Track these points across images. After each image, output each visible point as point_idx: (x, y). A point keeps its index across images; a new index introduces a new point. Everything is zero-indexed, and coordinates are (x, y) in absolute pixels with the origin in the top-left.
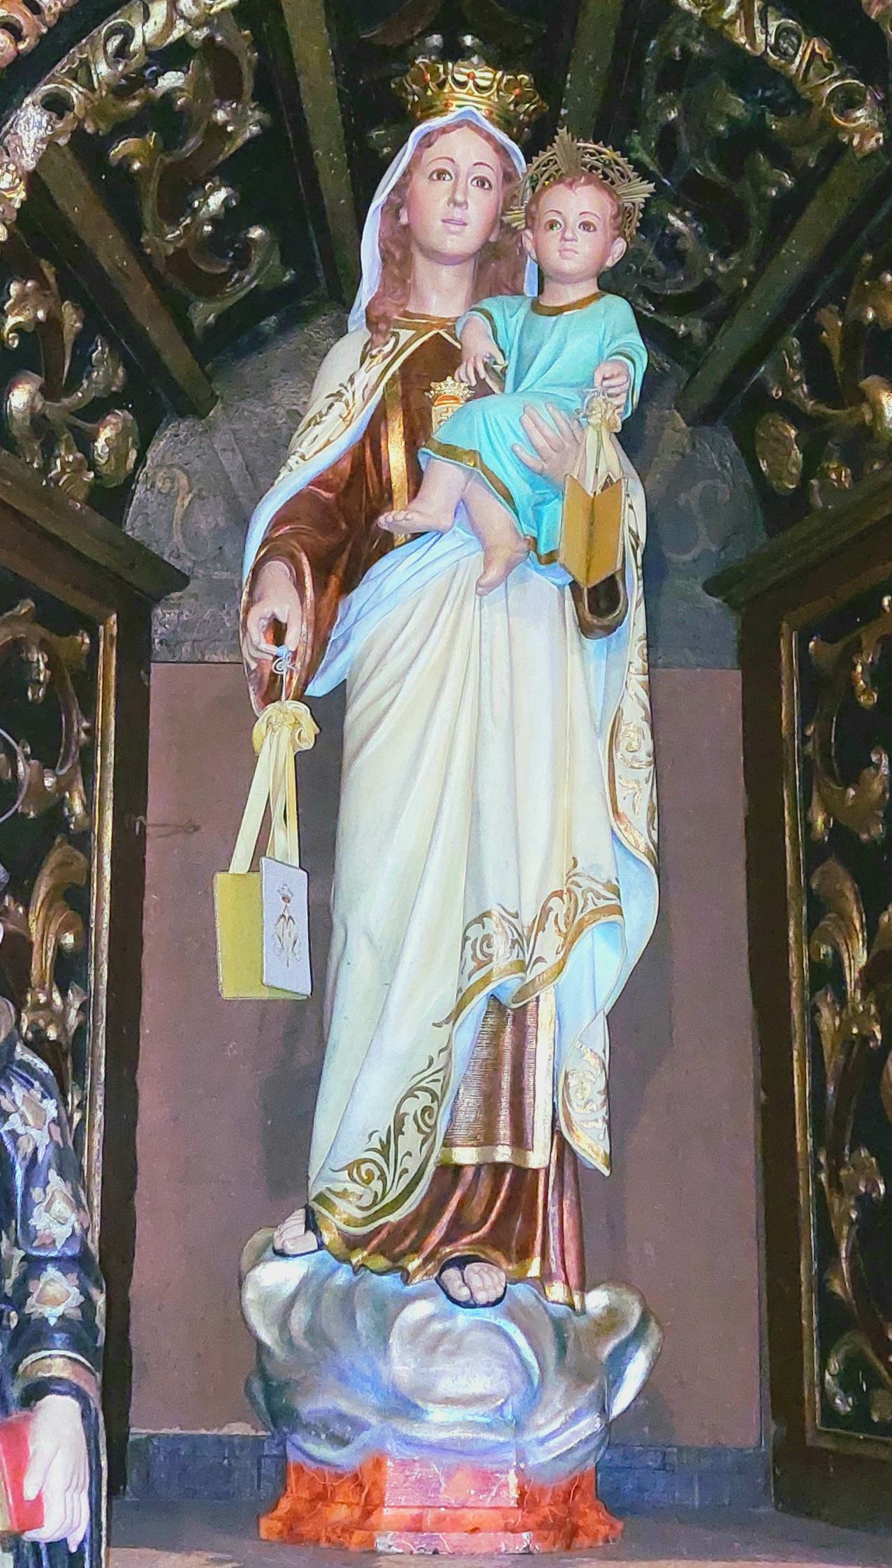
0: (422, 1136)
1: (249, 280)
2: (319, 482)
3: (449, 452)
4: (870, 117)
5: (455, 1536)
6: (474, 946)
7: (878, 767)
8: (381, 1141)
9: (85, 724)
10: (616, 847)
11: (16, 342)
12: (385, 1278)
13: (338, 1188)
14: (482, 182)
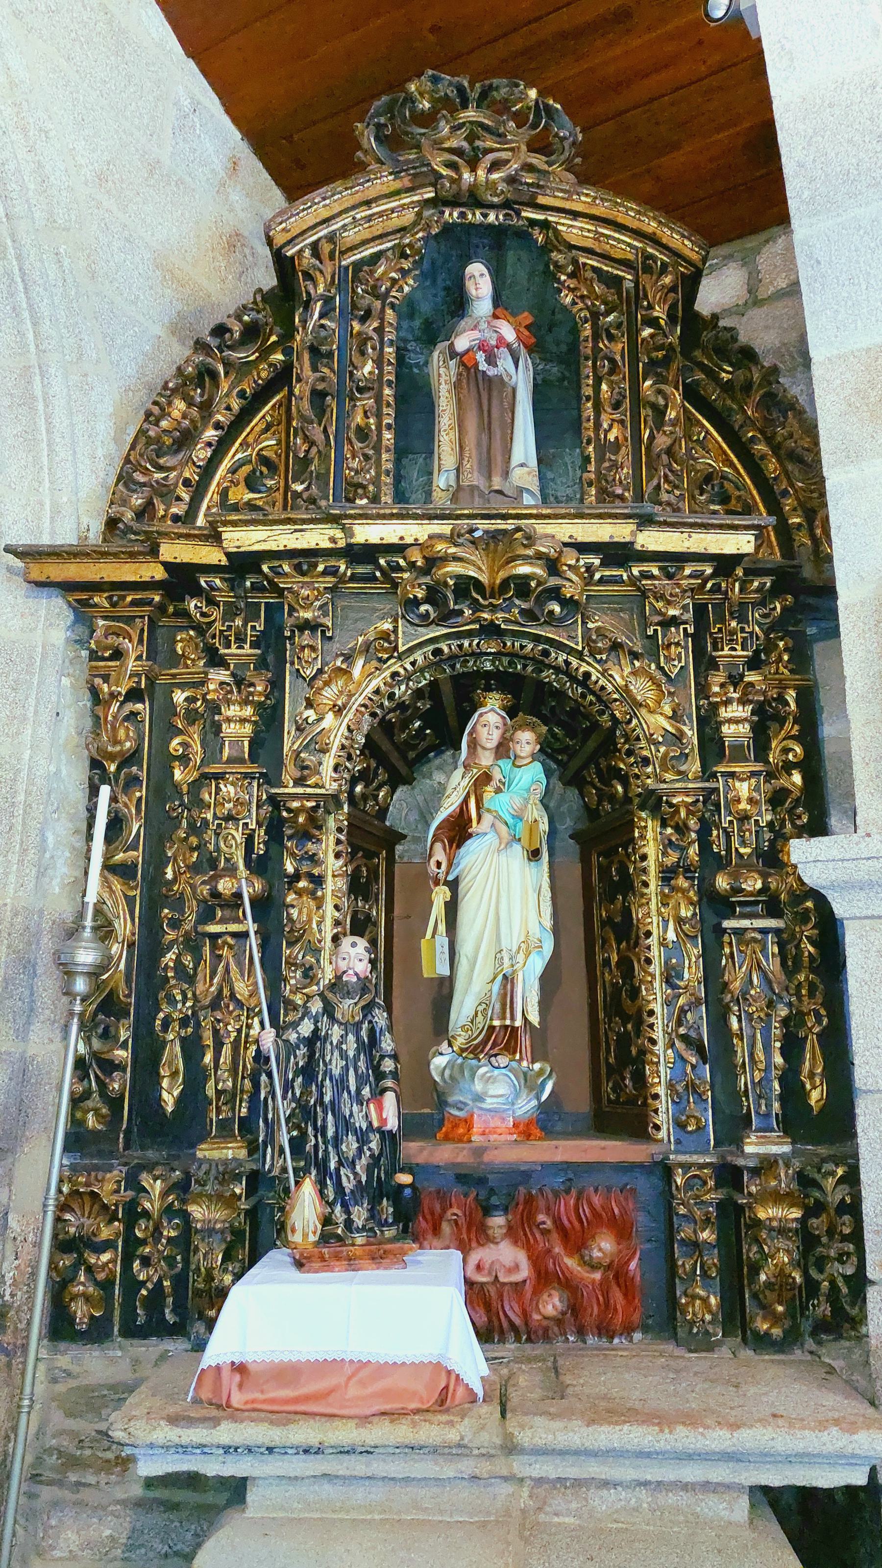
2: (450, 816)
3: (489, 811)
5: (495, 1136)
14: (497, 727)
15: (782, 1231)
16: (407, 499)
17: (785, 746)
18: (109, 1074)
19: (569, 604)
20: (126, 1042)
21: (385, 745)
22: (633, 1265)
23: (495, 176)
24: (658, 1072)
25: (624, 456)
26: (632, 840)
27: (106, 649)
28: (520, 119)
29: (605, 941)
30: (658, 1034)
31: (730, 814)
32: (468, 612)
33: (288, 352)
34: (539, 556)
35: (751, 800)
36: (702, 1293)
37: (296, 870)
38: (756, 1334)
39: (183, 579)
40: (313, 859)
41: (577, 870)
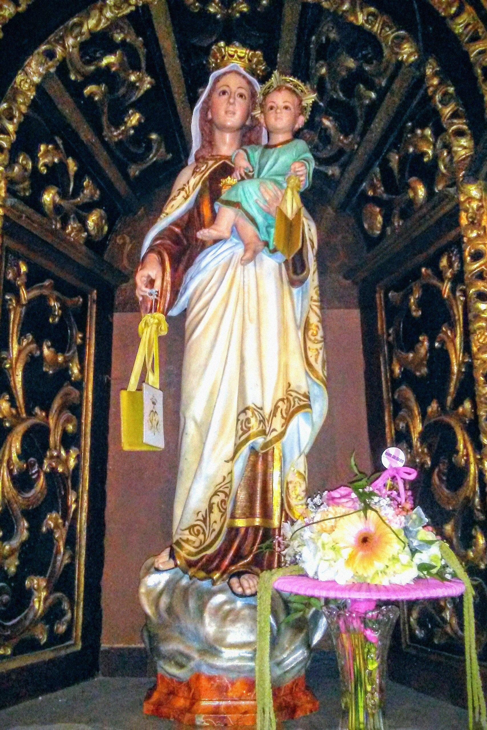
0: (221, 514)
1: (152, 158)
2: (175, 223)
4: (411, 47)
6: (242, 424)
7: (423, 342)
8: (203, 516)
9: (80, 335)
10: (310, 382)
11: (45, 171)
12: (204, 582)
13: (185, 537)
14: (241, 96)
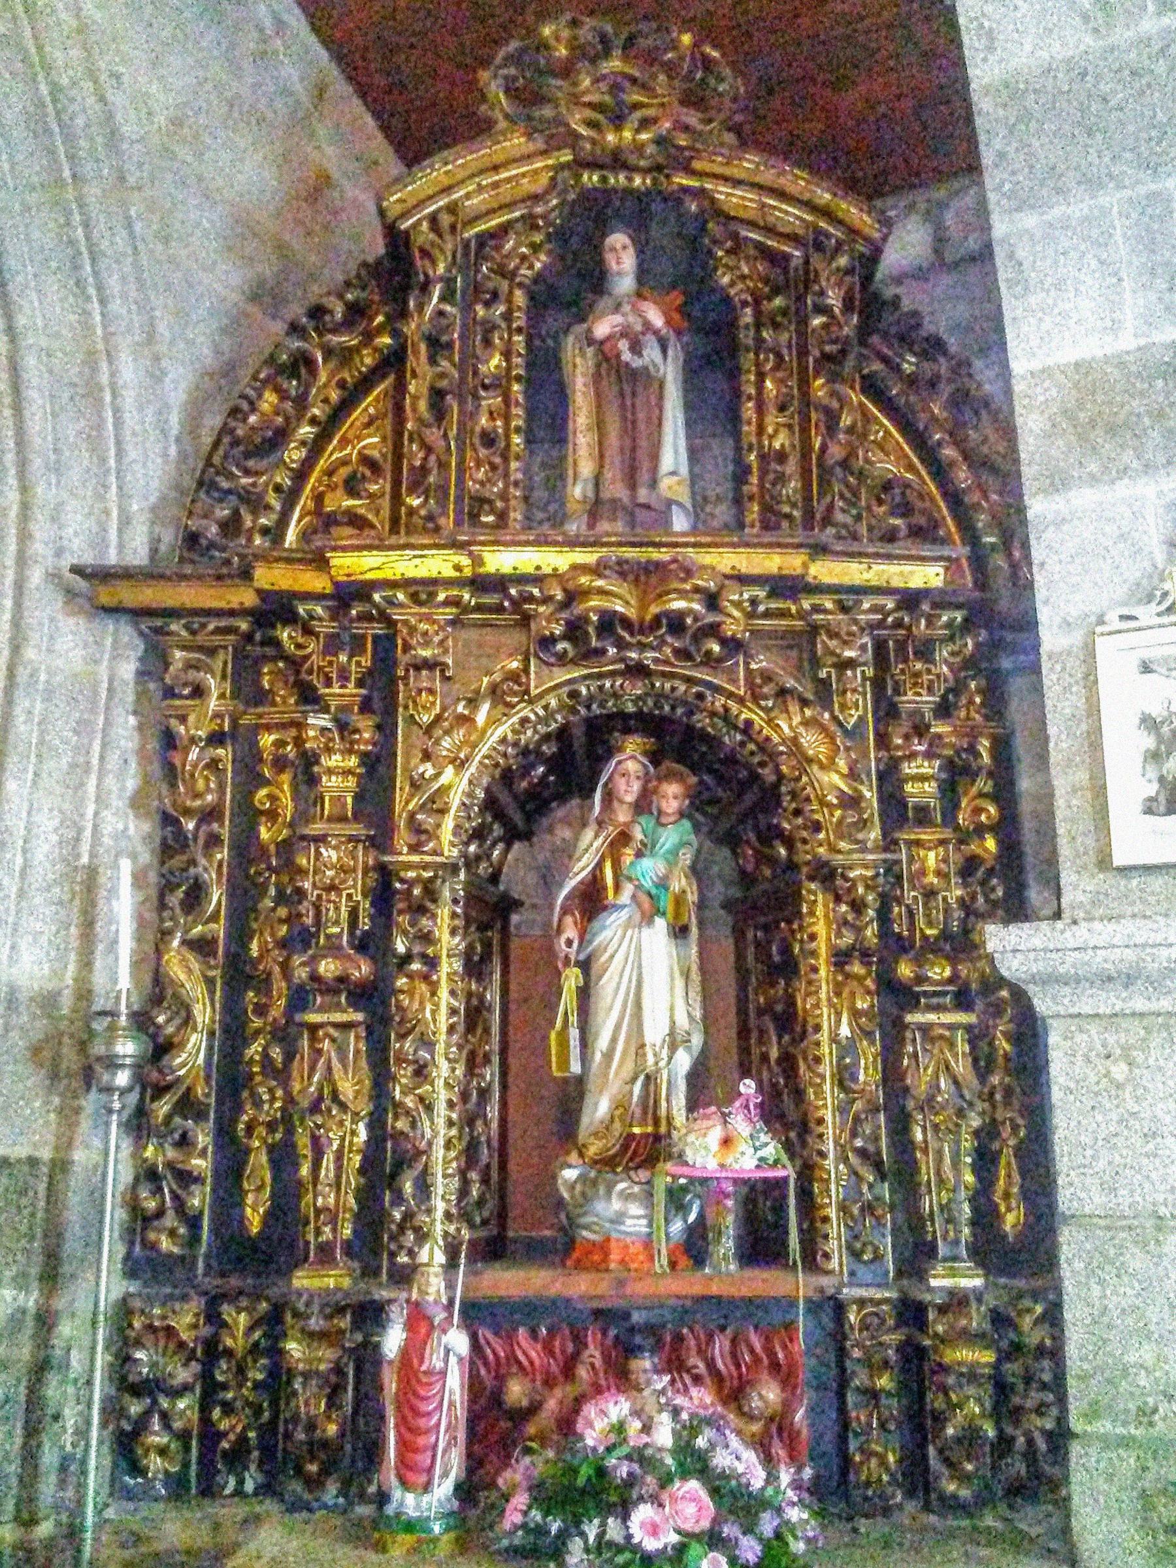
15: (972, 1376)
16: (545, 520)
17: (977, 806)
18: (186, 1187)
19: (733, 645)
20: (205, 1149)
21: (504, 797)
22: (799, 1416)
23: (644, 136)
24: (828, 1190)
25: (792, 466)
26: (799, 914)
27: (185, 685)
28: (670, 69)
29: (762, 1032)
30: (830, 1147)
31: (914, 888)
32: (612, 651)
33: (396, 333)
34: (697, 590)
35: (938, 873)
36: (879, 1449)
37: (409, 950)
38: (942, 1498)
39: (277, 609)
40: (427, 938)
41: (729, 944)
